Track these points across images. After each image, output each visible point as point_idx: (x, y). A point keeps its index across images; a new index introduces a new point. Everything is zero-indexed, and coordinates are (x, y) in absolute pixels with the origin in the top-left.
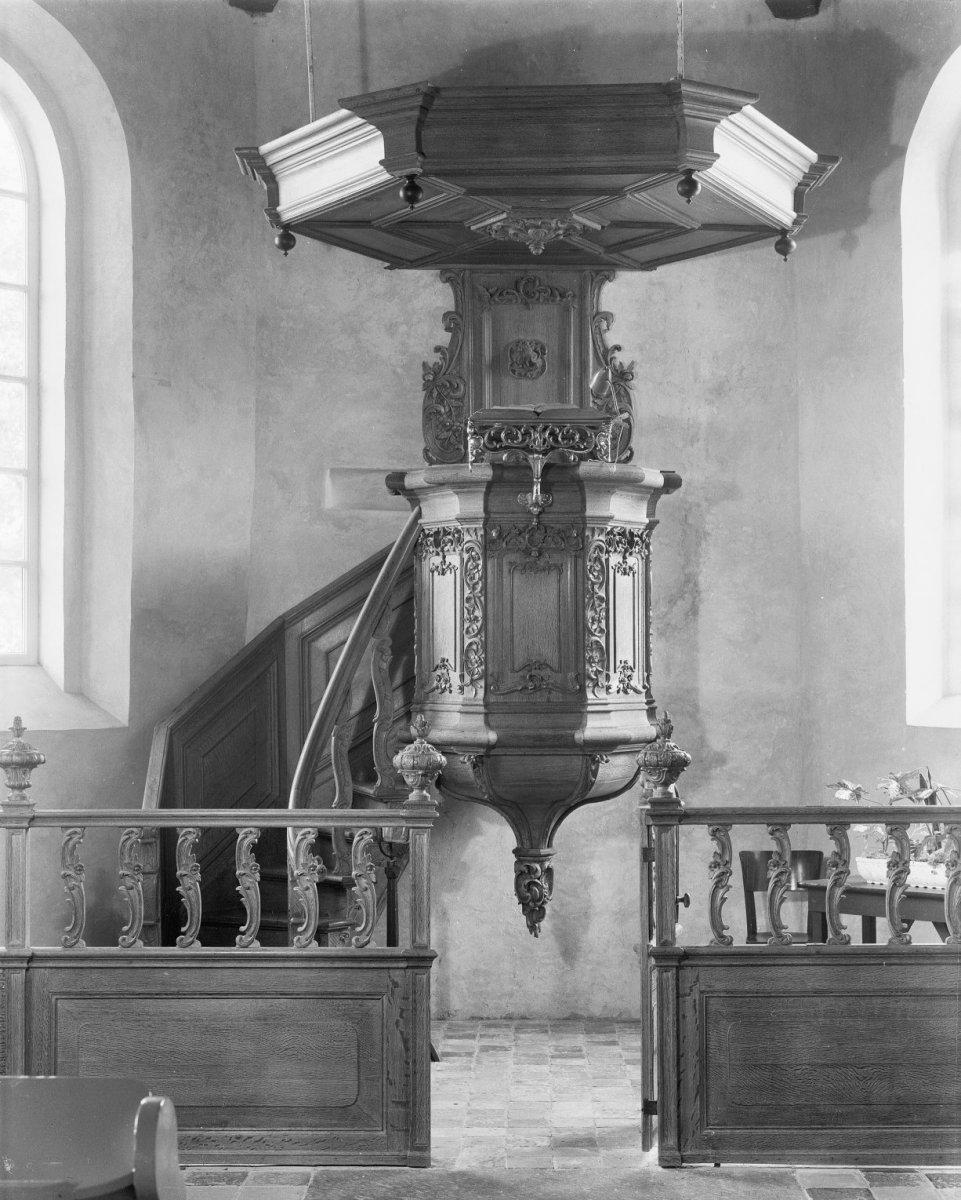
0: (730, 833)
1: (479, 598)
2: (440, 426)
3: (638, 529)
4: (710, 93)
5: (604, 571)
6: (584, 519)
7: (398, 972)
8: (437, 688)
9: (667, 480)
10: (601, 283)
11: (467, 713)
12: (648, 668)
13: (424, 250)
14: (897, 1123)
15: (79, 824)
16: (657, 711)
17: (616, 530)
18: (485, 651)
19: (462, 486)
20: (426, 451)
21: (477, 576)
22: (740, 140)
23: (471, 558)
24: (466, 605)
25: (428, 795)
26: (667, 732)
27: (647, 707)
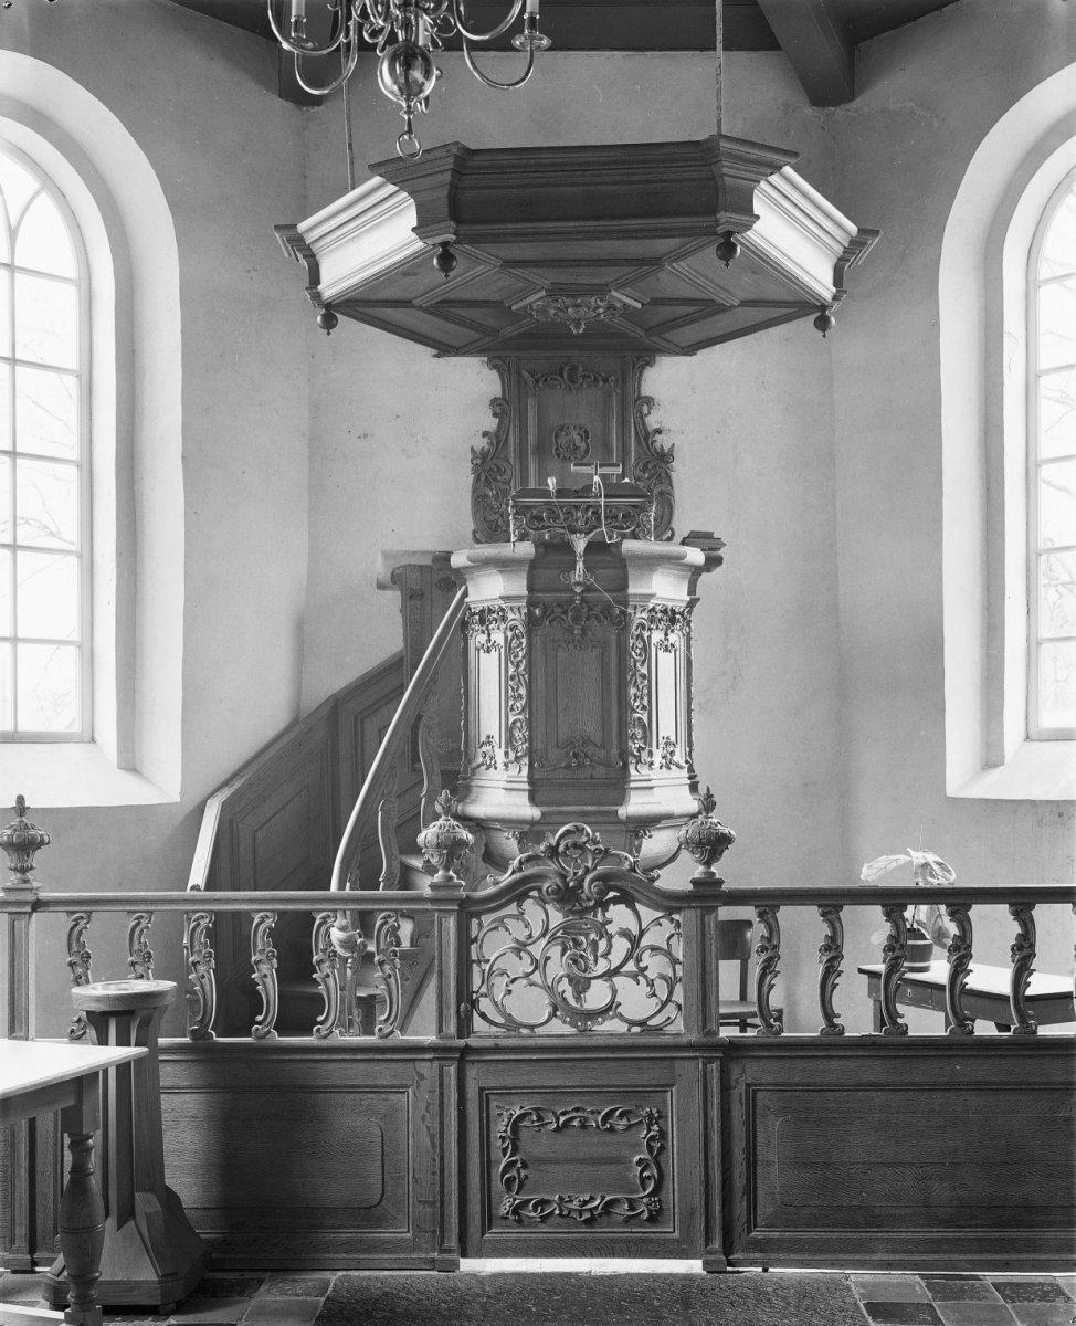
0: (777, 915)
1: (523, 676)
2: (488, 509)
3: (680, 606)
4: (748, 150)
5: (646, 649)
6: (627, 596)
7: (423, 1064)
8: (483, 764)
9: (708, 559)
10: (643, 368)
11: (511, 789)
12: (690, 743)
13: (467, 334)
14: (958, 1227)
15: (86, 909)
16: (699, 785)
17: (658, 608)
18: (530, 729)
19: (504, 565)
20: (474, 532)
21: (521, 654)
22: (780, 206)
23: (515, 636)
24: (511, 683)
25: (454, 875)
26: (709, 804)
27: (689, 782)
